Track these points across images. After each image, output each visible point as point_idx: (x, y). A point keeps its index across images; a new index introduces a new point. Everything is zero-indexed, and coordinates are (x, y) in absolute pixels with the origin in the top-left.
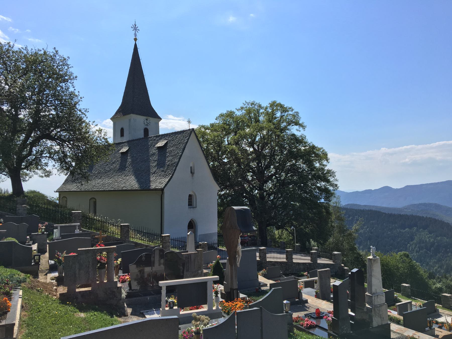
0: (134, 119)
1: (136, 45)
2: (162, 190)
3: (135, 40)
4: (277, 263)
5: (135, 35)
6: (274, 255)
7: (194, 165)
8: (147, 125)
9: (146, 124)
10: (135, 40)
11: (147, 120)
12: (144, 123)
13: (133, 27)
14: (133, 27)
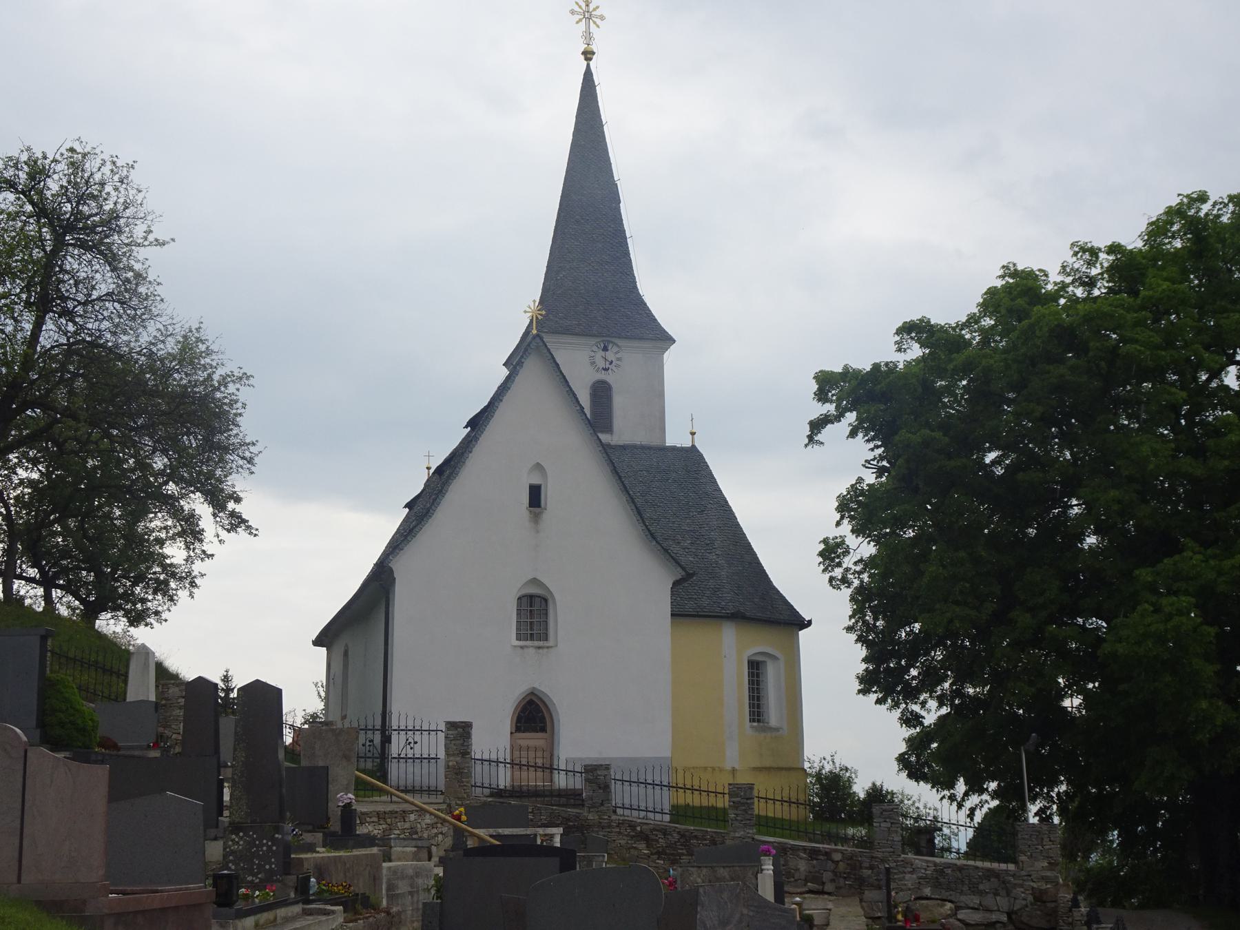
1: (588, 76)
3: (588, 55)
4: (665, 834)
5: (588, 37)
6: (658, 797)
8: (606, 369)
9: (601, 364)
10: (588, 55)
12: (593, 363)
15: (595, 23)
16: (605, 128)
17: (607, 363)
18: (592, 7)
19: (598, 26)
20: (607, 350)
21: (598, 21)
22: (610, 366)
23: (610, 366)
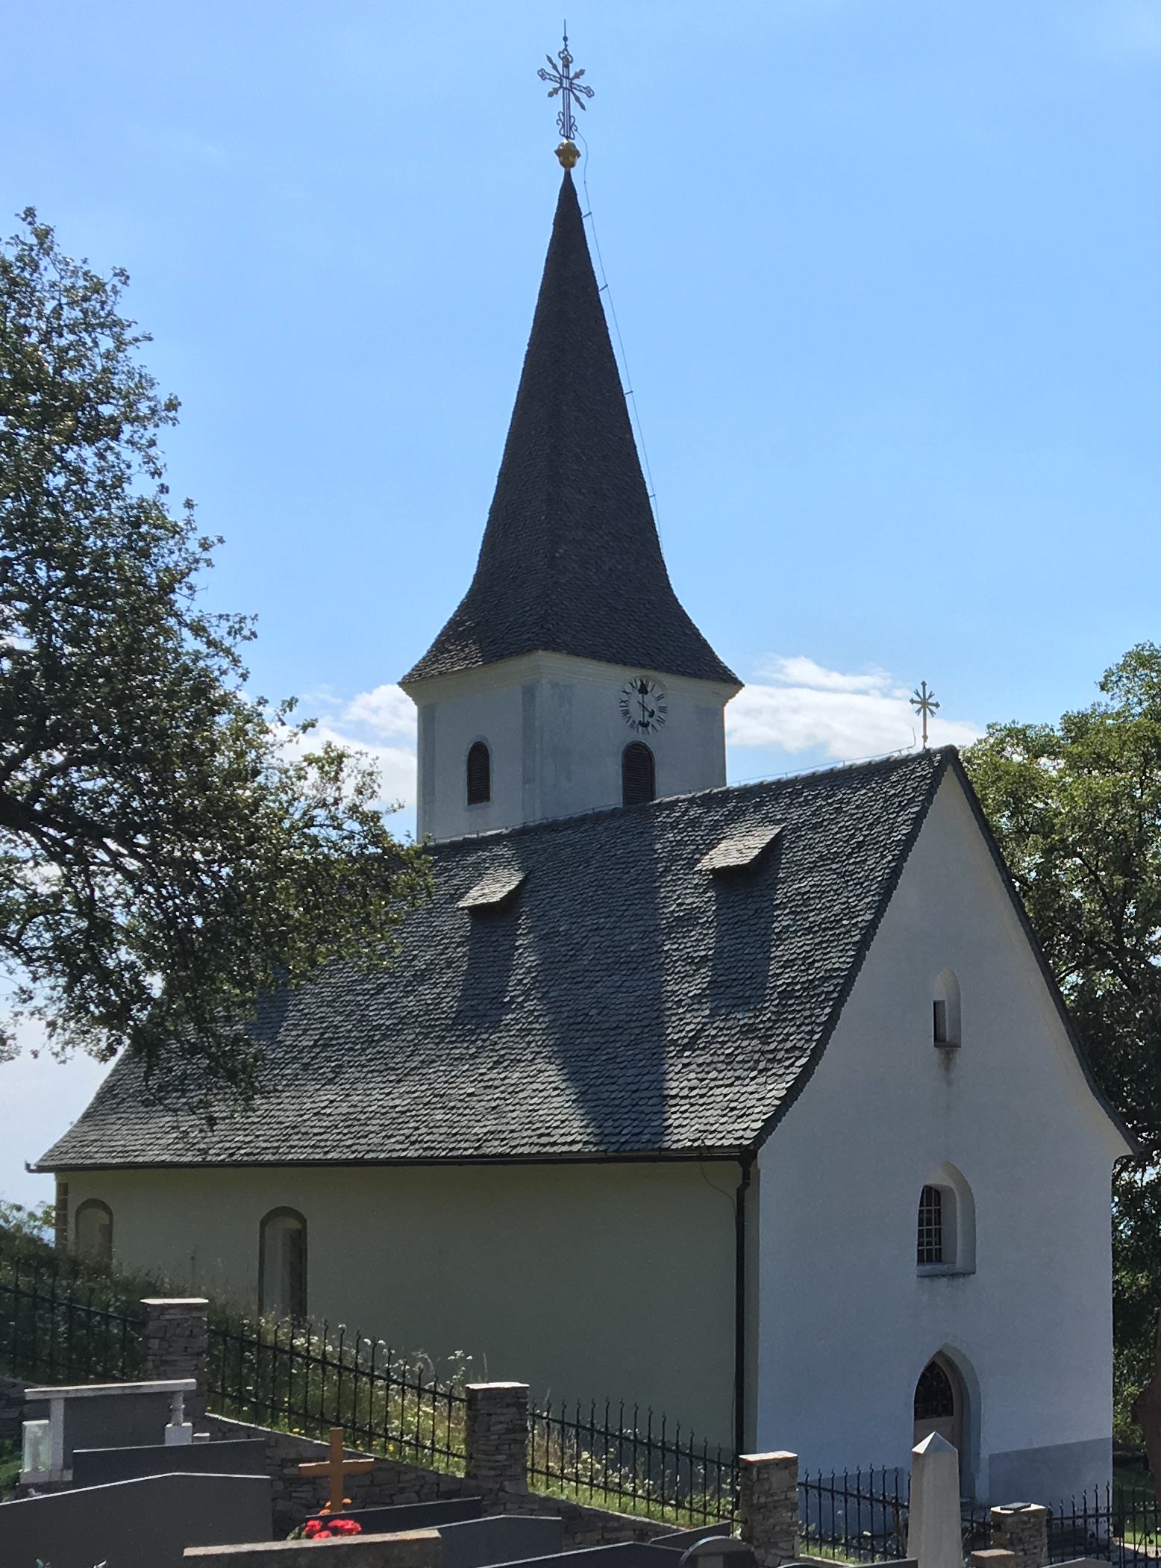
0: (555, 685)
1: (568, 195)
2: (745, 1156)
3: (568, 156)
5: (567, 125)
7: (959, 995)
8: (645, 725)
9: (637, 715)
10: (568, 156)
11: (643, 690)
12: (626, 713)
13: (550, 70)
14: (550, 70)
15: (577, 99)
16: (603, 296)
17: (646, 713)
18: (573, 69)
19: (583, 107)
20: (646, 693)
21: (583, 97)
22: (650, 720)
23: (650, 720)
